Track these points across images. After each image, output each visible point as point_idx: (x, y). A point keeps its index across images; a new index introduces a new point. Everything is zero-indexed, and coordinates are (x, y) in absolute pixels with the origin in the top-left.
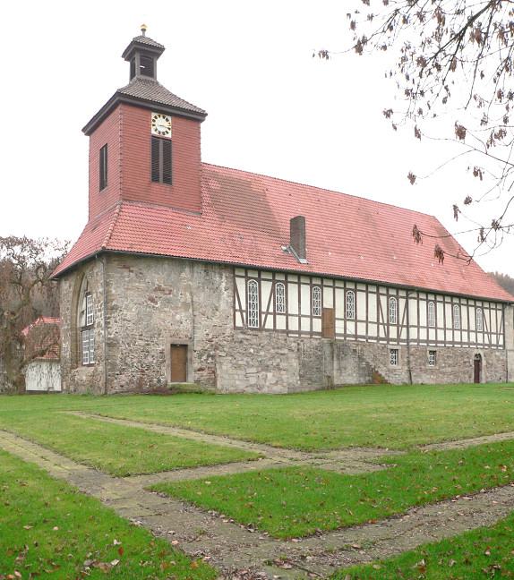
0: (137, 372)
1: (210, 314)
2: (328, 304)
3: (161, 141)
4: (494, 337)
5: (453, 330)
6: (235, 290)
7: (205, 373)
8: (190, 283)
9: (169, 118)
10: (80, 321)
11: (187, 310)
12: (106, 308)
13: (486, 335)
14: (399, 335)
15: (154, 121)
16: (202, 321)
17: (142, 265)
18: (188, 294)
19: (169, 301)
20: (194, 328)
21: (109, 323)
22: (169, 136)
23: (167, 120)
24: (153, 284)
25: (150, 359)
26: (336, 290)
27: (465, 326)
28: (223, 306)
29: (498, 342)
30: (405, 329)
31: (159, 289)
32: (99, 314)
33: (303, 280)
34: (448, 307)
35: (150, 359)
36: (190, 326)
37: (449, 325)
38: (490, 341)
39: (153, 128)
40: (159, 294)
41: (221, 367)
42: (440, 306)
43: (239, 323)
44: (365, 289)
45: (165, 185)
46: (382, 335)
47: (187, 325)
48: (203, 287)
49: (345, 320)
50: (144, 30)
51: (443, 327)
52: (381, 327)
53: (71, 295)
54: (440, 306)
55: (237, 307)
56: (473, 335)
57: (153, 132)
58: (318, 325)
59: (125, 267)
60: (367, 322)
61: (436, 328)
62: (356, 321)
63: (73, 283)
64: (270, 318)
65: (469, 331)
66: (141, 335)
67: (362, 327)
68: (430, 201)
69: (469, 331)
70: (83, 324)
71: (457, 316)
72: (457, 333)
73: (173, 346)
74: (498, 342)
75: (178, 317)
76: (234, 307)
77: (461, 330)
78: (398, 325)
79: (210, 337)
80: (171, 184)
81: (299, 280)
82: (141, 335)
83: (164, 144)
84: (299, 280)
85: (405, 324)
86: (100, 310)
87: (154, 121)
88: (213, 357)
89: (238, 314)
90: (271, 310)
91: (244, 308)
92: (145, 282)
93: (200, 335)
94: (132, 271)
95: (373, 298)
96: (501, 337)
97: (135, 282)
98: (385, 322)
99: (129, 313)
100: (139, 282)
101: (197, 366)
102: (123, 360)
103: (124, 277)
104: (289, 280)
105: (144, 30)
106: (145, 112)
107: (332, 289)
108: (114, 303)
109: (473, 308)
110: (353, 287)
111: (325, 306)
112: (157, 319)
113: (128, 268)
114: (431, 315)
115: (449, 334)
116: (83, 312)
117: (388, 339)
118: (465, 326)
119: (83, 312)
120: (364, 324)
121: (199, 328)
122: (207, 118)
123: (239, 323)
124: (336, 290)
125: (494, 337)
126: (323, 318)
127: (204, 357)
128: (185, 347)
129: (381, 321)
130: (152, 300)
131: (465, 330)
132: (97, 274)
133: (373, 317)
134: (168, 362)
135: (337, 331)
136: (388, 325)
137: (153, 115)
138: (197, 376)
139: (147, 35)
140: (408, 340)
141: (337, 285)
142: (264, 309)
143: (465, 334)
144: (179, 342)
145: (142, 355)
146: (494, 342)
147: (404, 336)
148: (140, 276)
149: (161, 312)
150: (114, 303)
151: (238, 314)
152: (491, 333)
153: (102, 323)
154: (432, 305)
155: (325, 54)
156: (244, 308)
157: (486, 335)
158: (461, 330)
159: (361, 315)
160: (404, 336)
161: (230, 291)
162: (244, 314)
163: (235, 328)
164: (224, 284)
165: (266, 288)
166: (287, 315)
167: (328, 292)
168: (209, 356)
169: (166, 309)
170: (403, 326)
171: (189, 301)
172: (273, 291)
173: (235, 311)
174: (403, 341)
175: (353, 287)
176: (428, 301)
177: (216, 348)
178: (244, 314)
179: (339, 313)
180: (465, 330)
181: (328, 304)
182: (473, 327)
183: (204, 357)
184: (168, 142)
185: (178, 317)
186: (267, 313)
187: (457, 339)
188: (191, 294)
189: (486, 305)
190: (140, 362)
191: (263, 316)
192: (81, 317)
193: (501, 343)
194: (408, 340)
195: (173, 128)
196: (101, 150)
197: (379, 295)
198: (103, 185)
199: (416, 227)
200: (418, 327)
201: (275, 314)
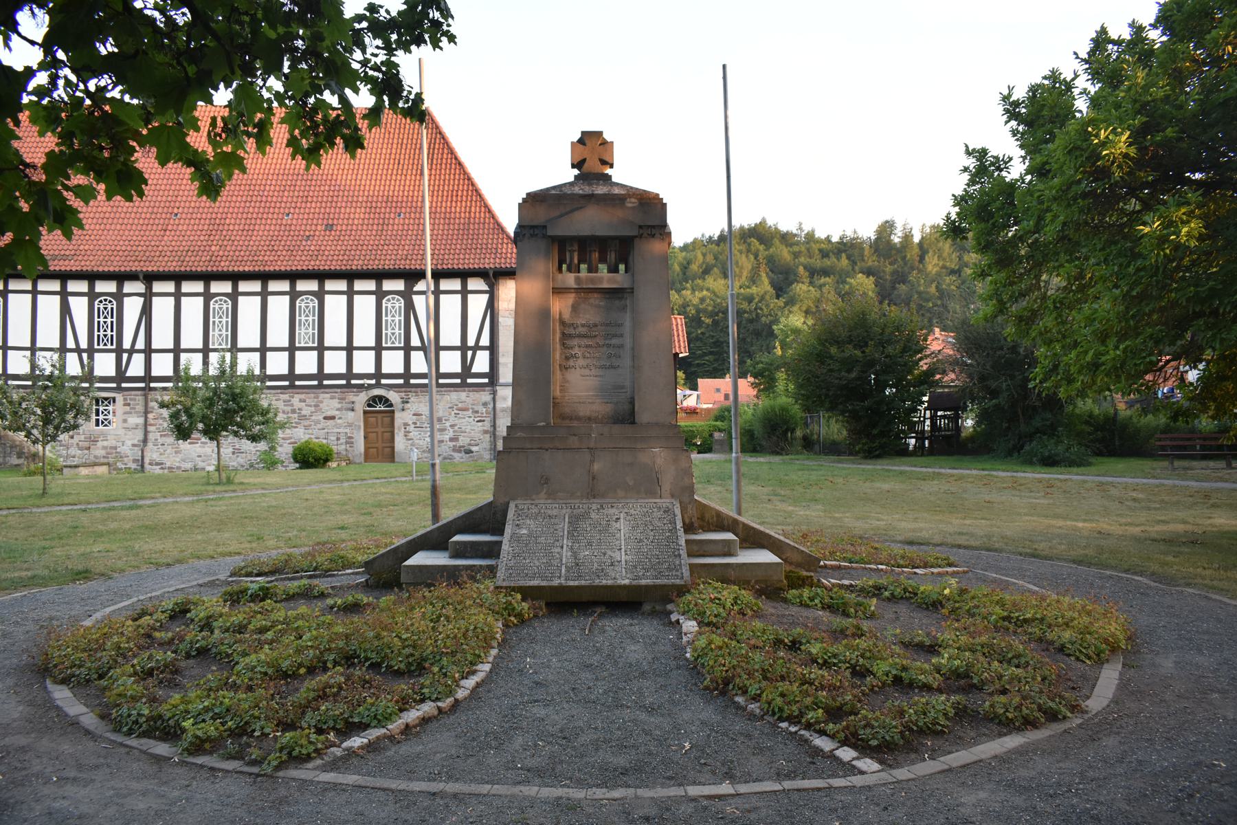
85: (140, 344)
104: (470, 288)
129: (71, 344)
136: (91, 351)
142: (127, 344)
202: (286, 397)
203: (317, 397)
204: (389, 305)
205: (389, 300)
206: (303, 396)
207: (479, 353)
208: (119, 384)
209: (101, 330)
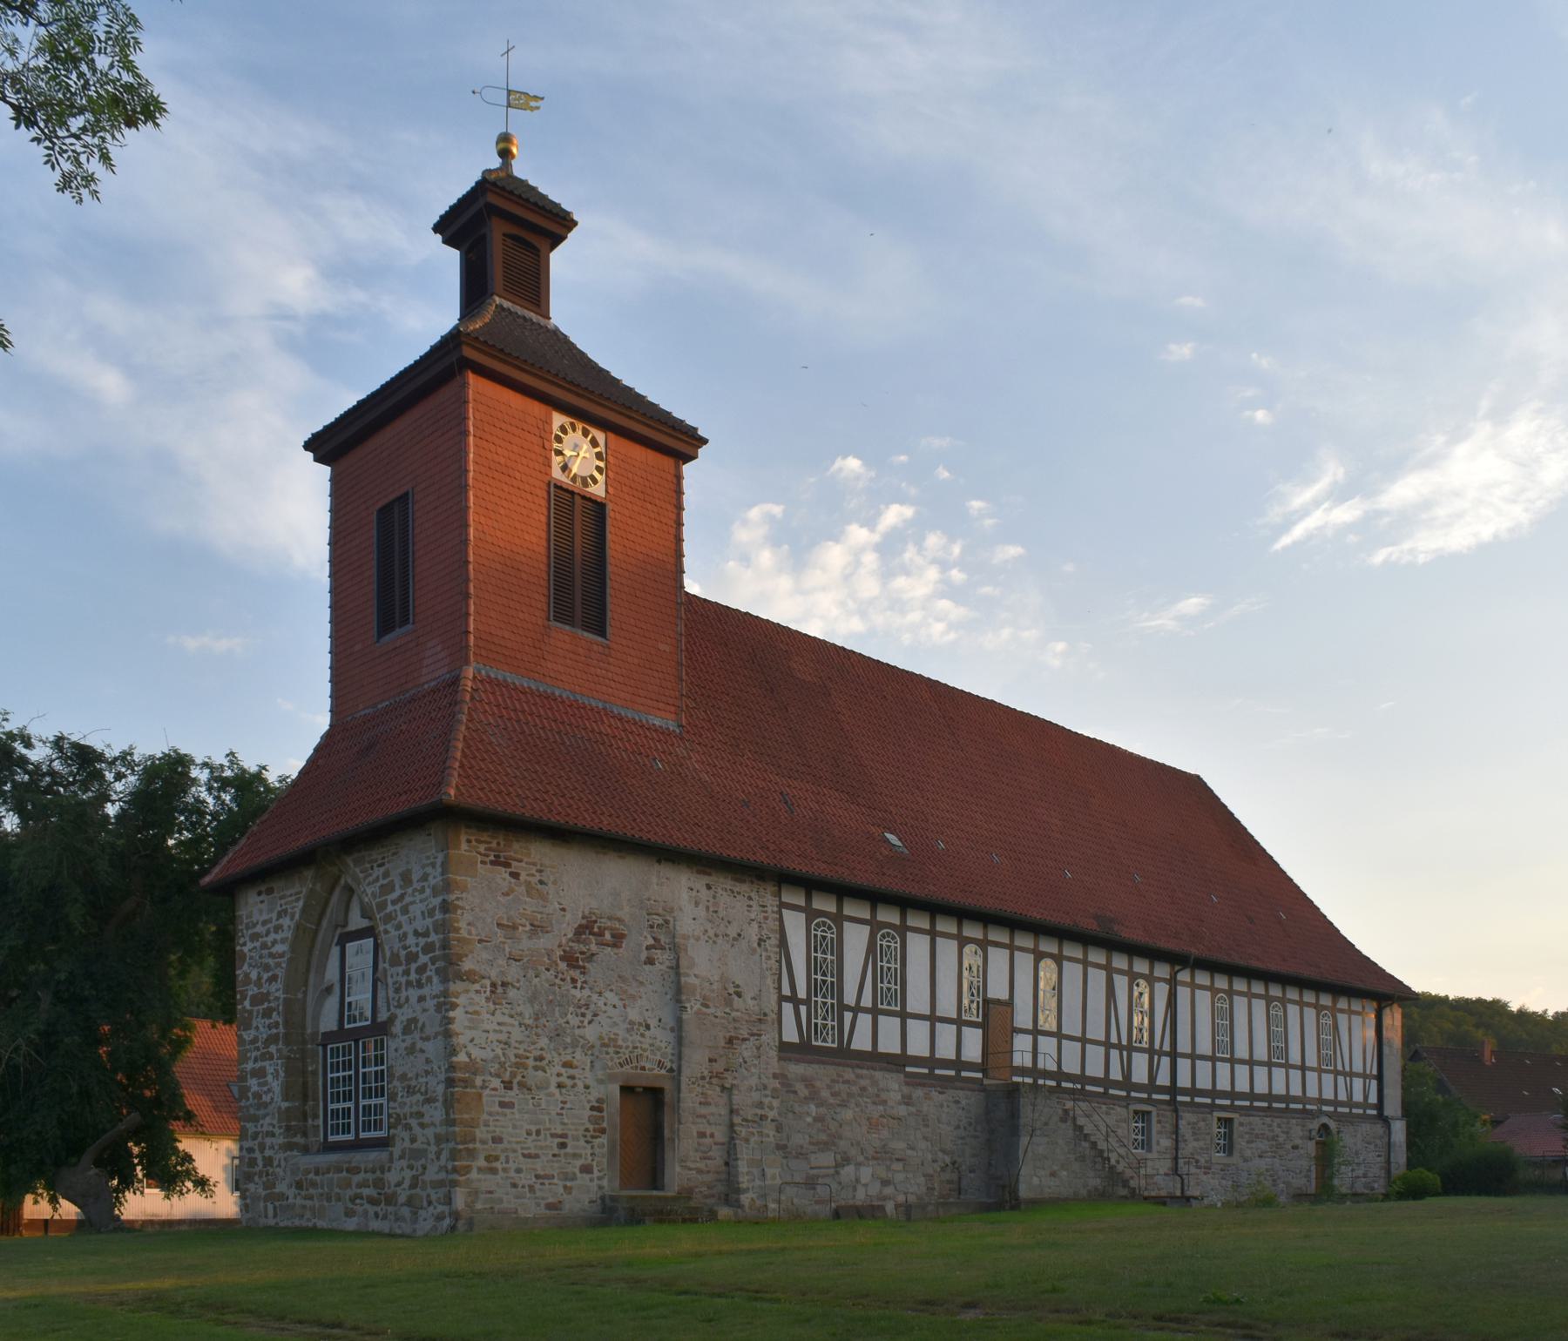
3: (578, 500)
5: (875, 1012)
9: (601, 437)
13: (1114, 1054)
14: (1152, 1076)
17: (540, 853)
22: (598, 490)
23: (594, 443)
26: (1017, 954)
29: (1366, 1097)
33: (850, 909)
38: (1127, 1073)
39: (557, 461)
44: (927, 926)
46: (1116, 1074)
50: (505, 154)
51: (1308, 1073)
57: (556, 473)
58: (973, 1048)
64: (865, 1020)
69: (1303, 1068)
74: (1366, 1097)
77: (1233, 1061)
78: (1151, 1051)
81: (933, 924)
84: (933, 924)
85: (1167, 1047)
87: (559, 440)
90: (867, 1001)
91: (802, 994)
98: (1124, 1042)
105: (505, 154)
106: (536, 408)
107: (927, 938)
109: (1263, 1003)
110: (926, 925)
111: (990, 995)
113: (507, 865)
114: (1330, 1040)
122: (702, 451)
124: (1017, 954)
125: (1358, 1084)
126: (984, 1025)
131: (1184, 1056)
135: (1018, 1060)
137: (558, 419)
139: (520, 169)
140: (1173, 1089)
141: (911, 922)
142: (849, 999)
147: (1163, 1079)
156: (802, 994)
157: (1114, 1054)
162: (803, 1009)
165: (856, 939)
166: (904, 1016)
167: (998, 958)
170: (1161, 1053)
172: (871, 949)
174: (1162, 1090)
175: (1055, 950)
178: (803, 1009)
180: (1184, 1056)
181: (998, 990)
182: (1311, 1061)
184: (598, 509)
186: (857, 1009)
189: (1292, 994)
191: (848, 1016)
192: (319, 1003)
193: (1373, 1099)
194: (1173, 1089)
197: (1109, 969)
199: (404, 498)
200: (933, 1019)
202: (1268, 1120)
203: (1288, 1123)
204: (884, 943)
207: (860, 1015)
208: (931, 1075)
209: (885, 982)
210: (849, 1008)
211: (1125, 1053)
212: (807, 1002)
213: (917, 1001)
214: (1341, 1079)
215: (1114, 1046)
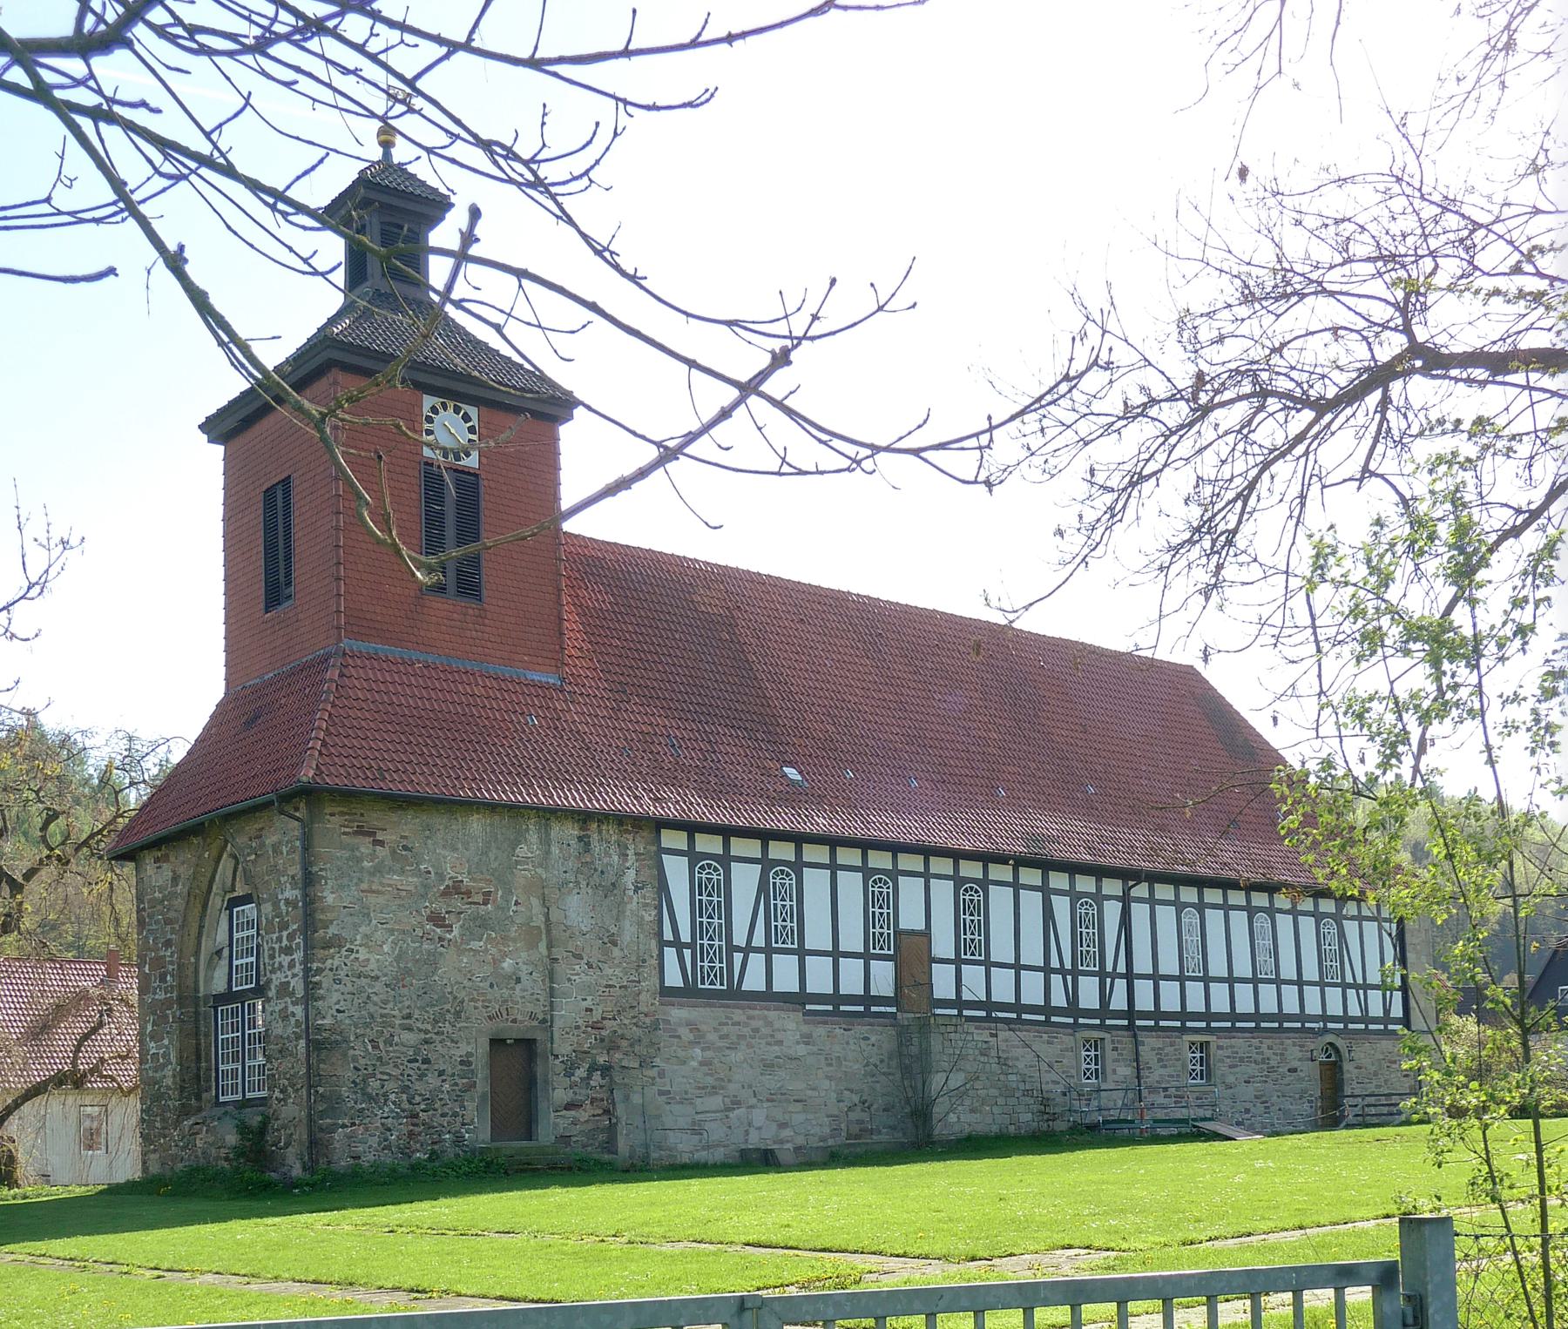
0: (398, 1116)
1: (594, 955)
2: (911, 919)
4: (1375, 997)
6: (663, 887)
7: (583, 1115)
8: (539, 870)
9: (473, 412)
10: (209, 980)
11: (532, 945)
12: (309, 946)
13: (1351, 993)
14: (1104, 999)
15: (430, 420)
16: (576, 975)
18: (535, 902)
19: (483, 924)
20: (552, 993)
21: (318, 985)
22: (472, 461)
23: (466, 418)
24: (441, 877)
25: (433, 1080)
27: (1289, 971)
28: (629, 931)
29: (1387, 1011)
30: (1121, 984)
31: (456, 889)
32: (286, 960)
34: (1239, 919)
35: (433, 1080)
36: (540, 990)
37: (1311, 973)
38: (1365, 1008)
39: (475, 422)
40: (457, 903)
41: (627, 1098)
42: (1214, 918)
43: (674, 978)
45: (463, 602)
47: (533, 984)
48: (577, 883)
49: (958, 962)
52: (1056, 980)
53: (179, 903)
54: (1214, 918)
55: (668, 935)
56: (1244, 993)
58: (884, 977)
59: (360, 832)
60: (1018, 967)
61: (1206, 980)
62: (988, 964)
63: (185, 872)
64: (757, 961)
65: (1300, 983)
66: (409, 1016)
67: (1220, 992)
68: (1175, 651)
69: (1300, 983)
70: (219, 985)
71: (1264, 943)
72: (1268, 992)
73: (497, 1043)
74: (1387, 1011)
75: (507, 964)
76: (660, 933)
77: (1279, 982)
78: (1102, 974)
79: (597, 1015)
80: (479, 598)
82: (409, 1016)
83: (459, 484)
85: (1122, 968)
86: (288, 951)
88: (606, 1070)
89: (669, 954)
90: (759, 940)
91: (685, 937)
92: (418, 873)
93: (568, 1012)
94: (381, 843)
95: (1032, 903)
96: (1398, 995)
97: (391, 870)
98: (1068, 966)
99: (374, 957)
100: (403, 872)
101: (560, 1095)
102: (360, 1086)
103: (359, 860)
108: (332, 930)
112: (451, 967)
115: (1312, 994)
116: (219, 953)
117: (1073, 1008)
118: (1289, 971)
119: (219, 953)
120: (1162, 971)
121: (566, 995)
123: (674, 978)
125: (1375, 997)
127: (581, 1073)
128: (527, 1046)
129: (1055, 963)
130: (437, 919)
132: (276, 849)
133: (1032, 953)
134: (482, 1087)
136: (1075, 973)
137: (428, 401)
138: (562, 1123)
142: (740, 939)
143: (1290, 992)
144: (512, 1033)
145: (412, 1070)
146: (1376, 1010)
148: (404, 854)
149: (461, 952)
150: (332, 930)
151: (669, 954)
152: (1366, 987)
153: (297, 985)
154: (1262, 920)
155: (1296, 85)
156: (685, 937)
158: (1279, 982)
159: (1002, 950)
160: (1119, 1002)
161: (649, 893)
162: (687, 953)
163: (666, 992)
164: (631, 875)
168: (593, 1068)
169: (475, 945)
171: (539, 921)
173: (663, 944)
176: (1180, 906)
177: (612, 1047)
178: (687, 953)
179: (943, 944)
181: (911, 919)
182: (1311, 973)
183: (581, 1073)
184: (468, 482)
185: (507, 964)
186: (748, 949)
187: (1335, 1008)
188: (544, 900)
190: (405, 1089)
191: (738, 957)
192: (211, 966)
193: (1397, 1012)
195: (484, 431)
196: (269, 494)
198: (276, 591)
201: (768, 951)
205: (1082, 905)
206: (1269, 1042)
209: (780, 920)
210: (739, 949)
211: (1069, 978)
212: (692, 946)
213: (816, 935)
214: (1351, 993)
215: (1350, 986)
